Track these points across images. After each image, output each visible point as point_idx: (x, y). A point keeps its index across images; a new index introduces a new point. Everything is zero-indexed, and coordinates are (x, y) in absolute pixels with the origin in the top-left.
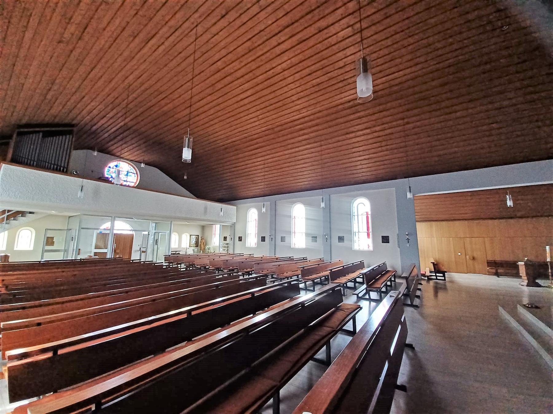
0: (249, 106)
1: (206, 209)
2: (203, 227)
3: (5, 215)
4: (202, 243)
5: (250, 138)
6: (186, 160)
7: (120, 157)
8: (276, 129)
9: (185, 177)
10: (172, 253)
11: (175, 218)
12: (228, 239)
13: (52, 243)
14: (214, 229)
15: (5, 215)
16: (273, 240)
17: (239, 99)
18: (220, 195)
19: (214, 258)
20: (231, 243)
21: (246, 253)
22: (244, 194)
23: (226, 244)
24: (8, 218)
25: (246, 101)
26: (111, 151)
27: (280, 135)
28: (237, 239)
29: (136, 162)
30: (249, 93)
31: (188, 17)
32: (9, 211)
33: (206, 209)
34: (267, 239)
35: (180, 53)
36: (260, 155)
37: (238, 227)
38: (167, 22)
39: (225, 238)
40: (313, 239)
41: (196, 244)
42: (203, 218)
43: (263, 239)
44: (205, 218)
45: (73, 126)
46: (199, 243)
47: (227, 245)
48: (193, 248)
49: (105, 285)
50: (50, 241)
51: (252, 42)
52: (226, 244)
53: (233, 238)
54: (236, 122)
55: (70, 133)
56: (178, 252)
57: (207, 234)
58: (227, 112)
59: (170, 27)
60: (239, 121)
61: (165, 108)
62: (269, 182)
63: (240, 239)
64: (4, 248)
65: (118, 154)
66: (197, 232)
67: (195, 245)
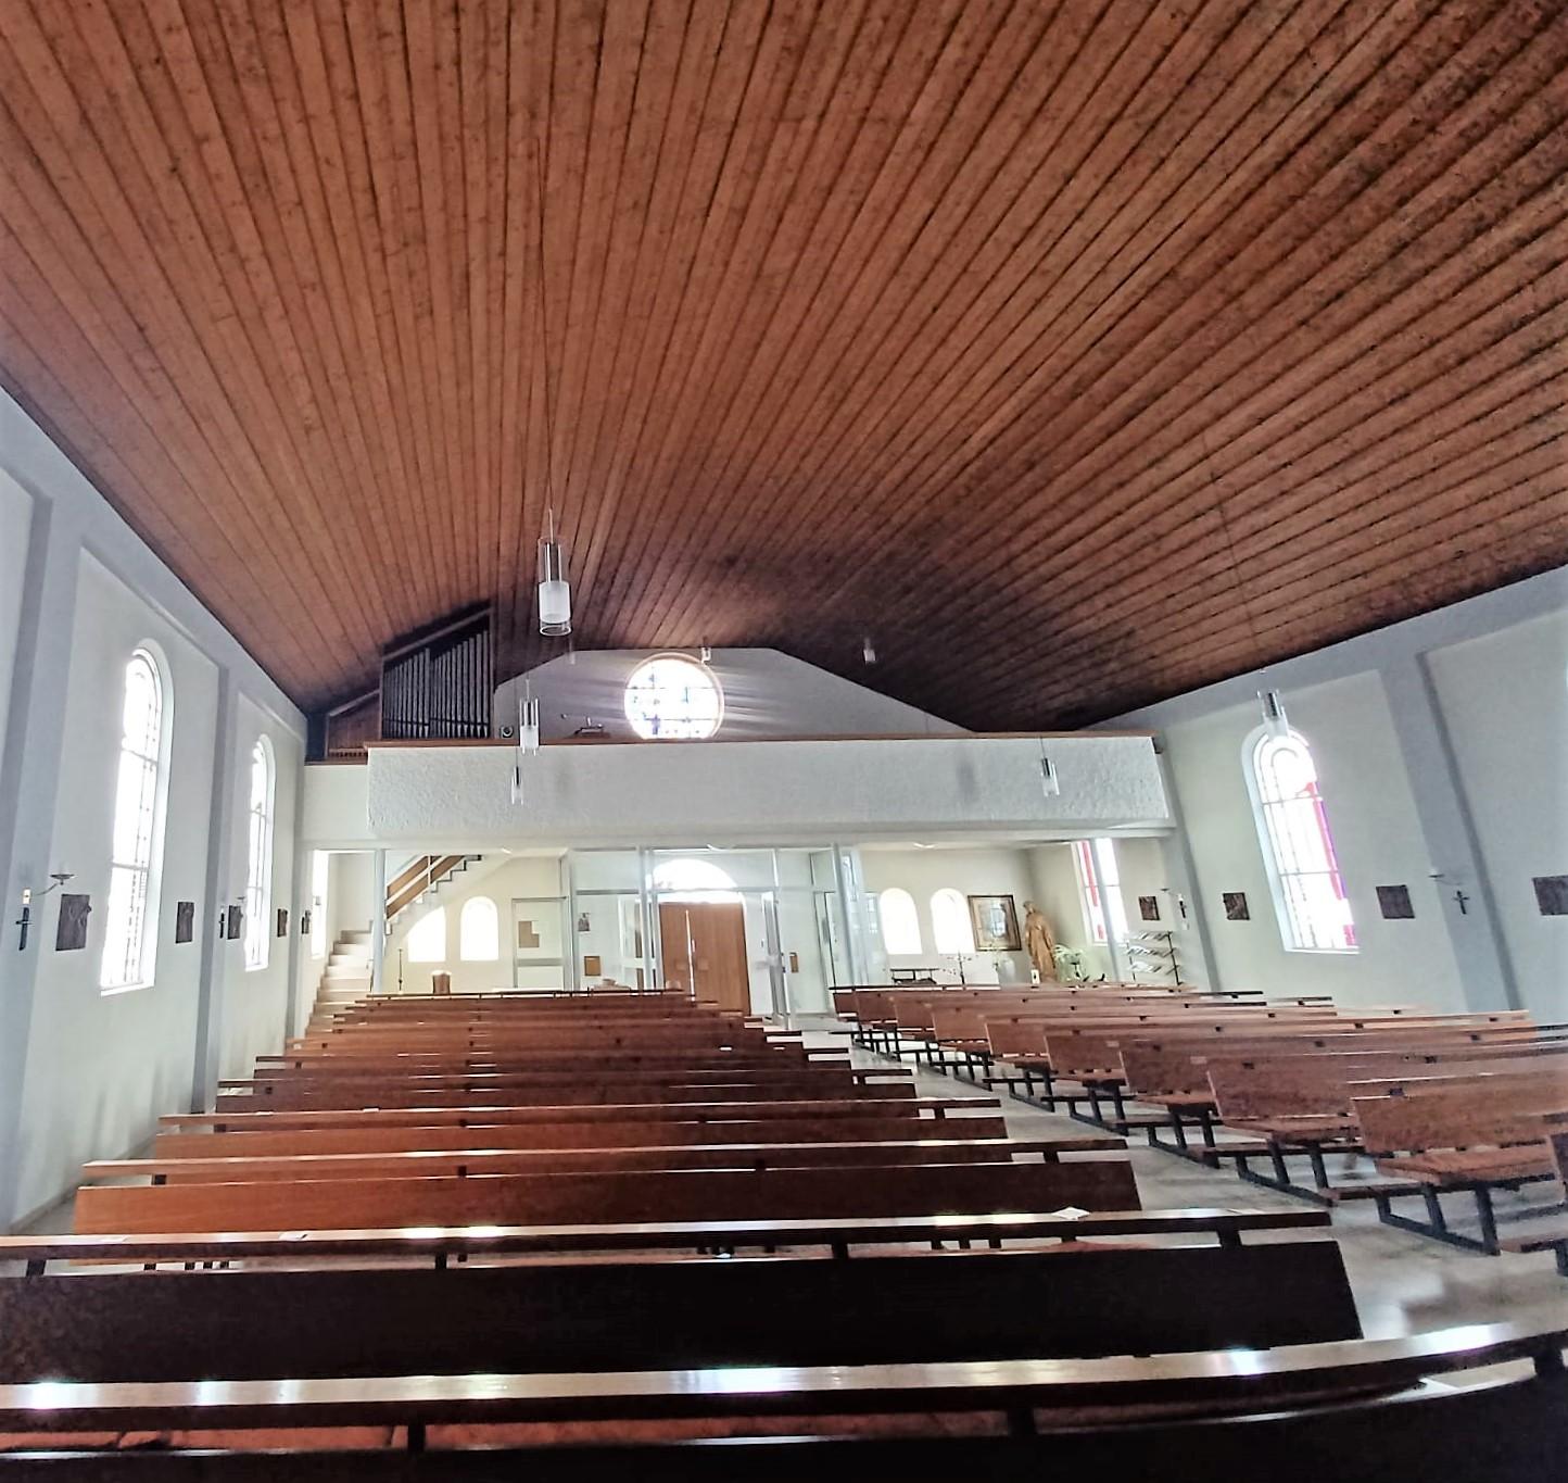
0: (956, 256)
1: (966, 774)
2: (1028, 859)
3: (428, 871)
4: (1037, 933)
5: (1069, 380)
6: (555, 627)
7: (645, 648)
8: (1190, 269)
9: (869, 656)
10: (898, 975)
11: (862, 832)
12: (1165, 906)
13: (534, 941)
14: (1081, 866)
15: (428, 871)
16: (1476, 903)
17: (895, 255)
18: (1061, 695)
19: (1493, 1014)
20: (1187, 929)
21: (1279, 990)
22: (1192, 656)
23: (1160, 937)
24: (434, 875)
25: (932, 241)
26: (622, 640)
27: (1237, 285)
28: (1217, 911)
29: (725, 647)
30: (918, 206)
31: (106, 282)
32: (433, 859)
33: (966, 774)
34: (1423, 897)
35: (574, 262)
36: (1172, 434)
37: (1206, 839)
38: (465, 216)
39: (1149, 908)
40: (1390, 898)
41: (1007, 936)
42: (960, 815)
43: (1396, 902)
44: (974, 817)
45: (486, 604)
46: (1025, 935)
47: (1164, 945)
48: (990, 957)
49: (665, 1083)
50: (527, 936)
51: (402, 158)
52: (1160, 937)
53: (1189, 903)
54: (946, 356)
55: (482, 625)
56: (925, 975)
57: (1054, 886)
58: (877, 337)
59: (486, 220)
60: (957, 341)
61: (670, 447)
62: (1313, 559)
63: (1236, 906)
64: (441, 957)
65: (644, 640)
66: (1001, 880)
67: (1002, 945)
